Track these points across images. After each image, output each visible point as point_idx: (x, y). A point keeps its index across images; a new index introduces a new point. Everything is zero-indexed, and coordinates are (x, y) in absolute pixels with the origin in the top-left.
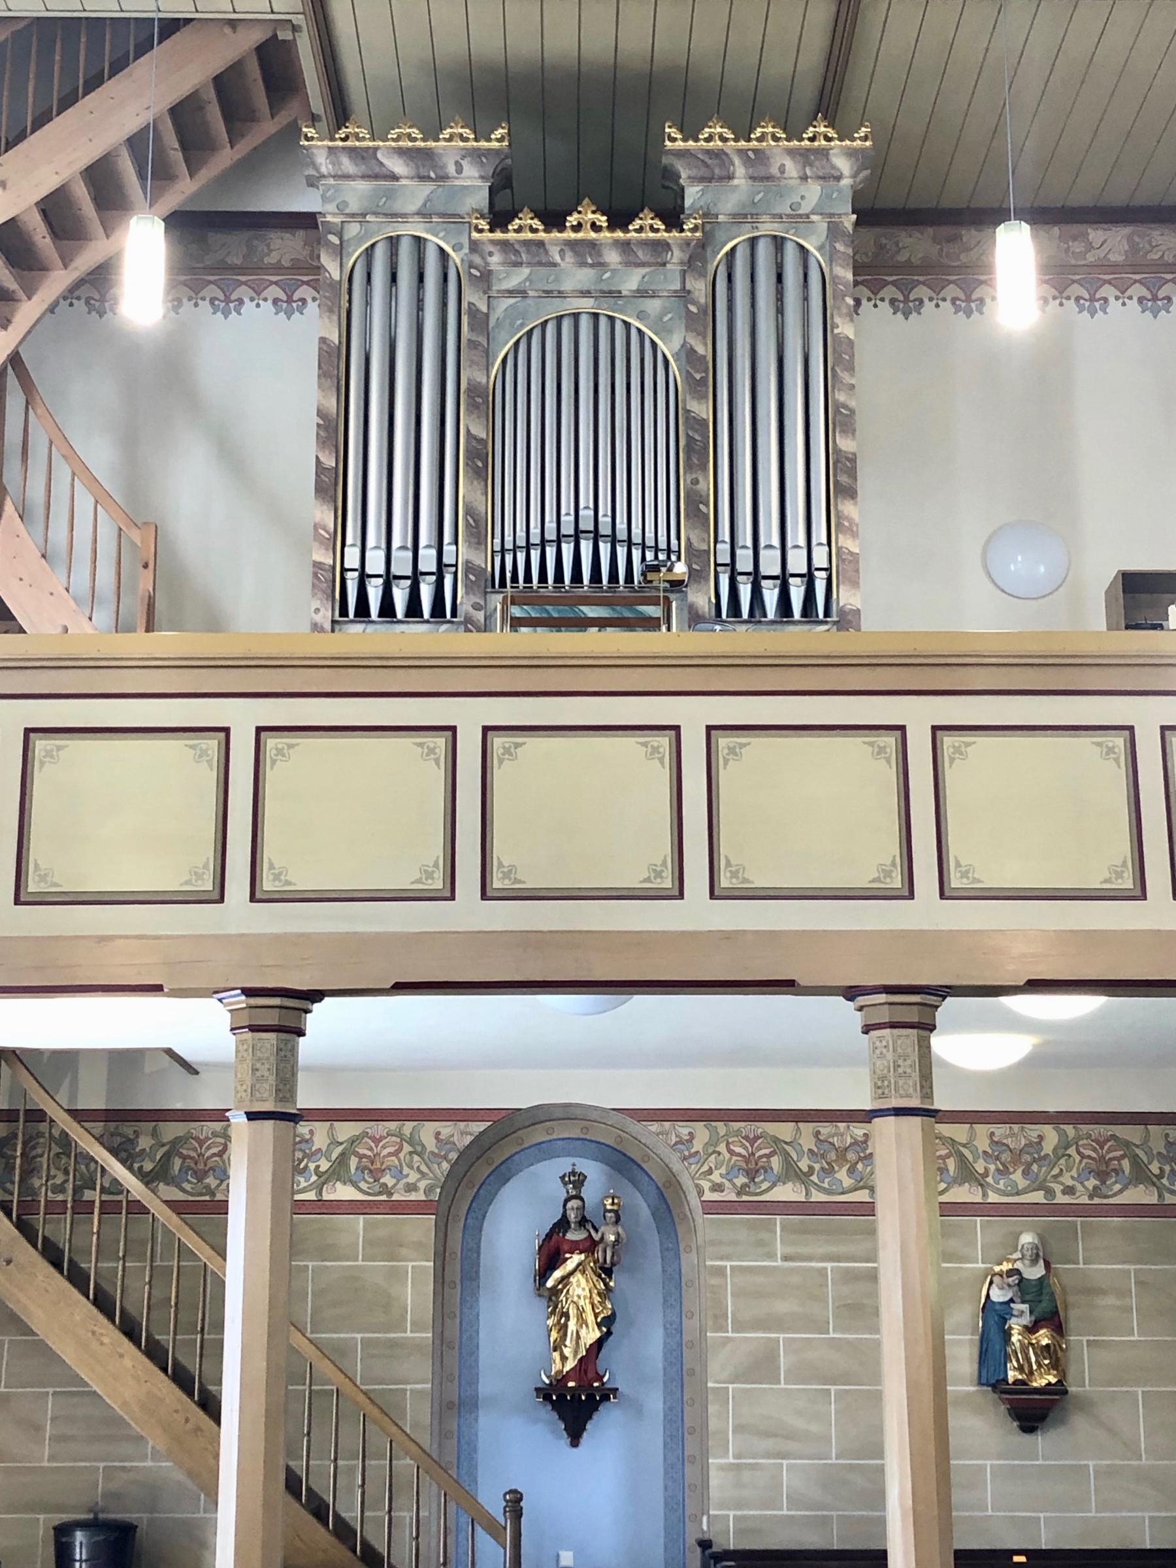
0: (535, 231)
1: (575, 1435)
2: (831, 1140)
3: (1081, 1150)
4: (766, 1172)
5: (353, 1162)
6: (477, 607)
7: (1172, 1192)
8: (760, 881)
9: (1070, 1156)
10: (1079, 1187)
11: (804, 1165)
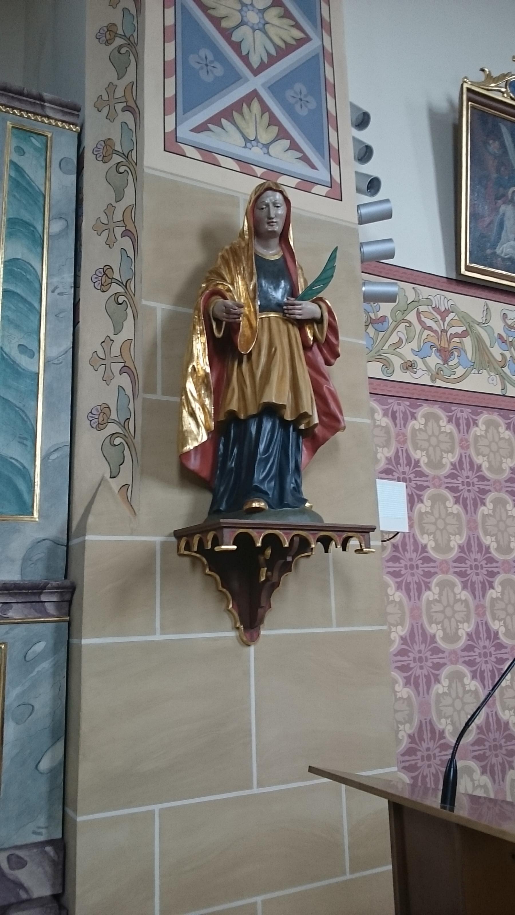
3: (423, 319)
7: (514, 384)
8: (174, 93)
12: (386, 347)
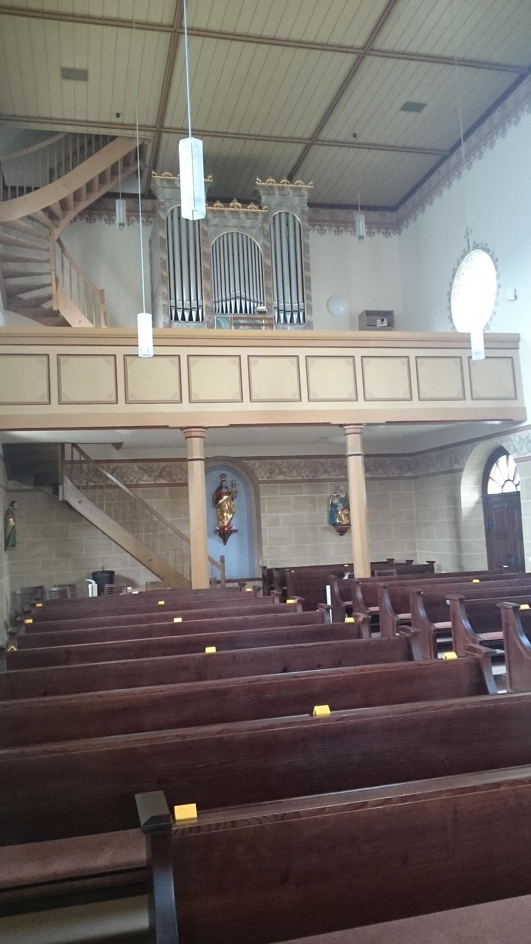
0: (221, 207)
1: (225, 541)
5: (164, 473)
6: (210, 318)
11: (284, 470)
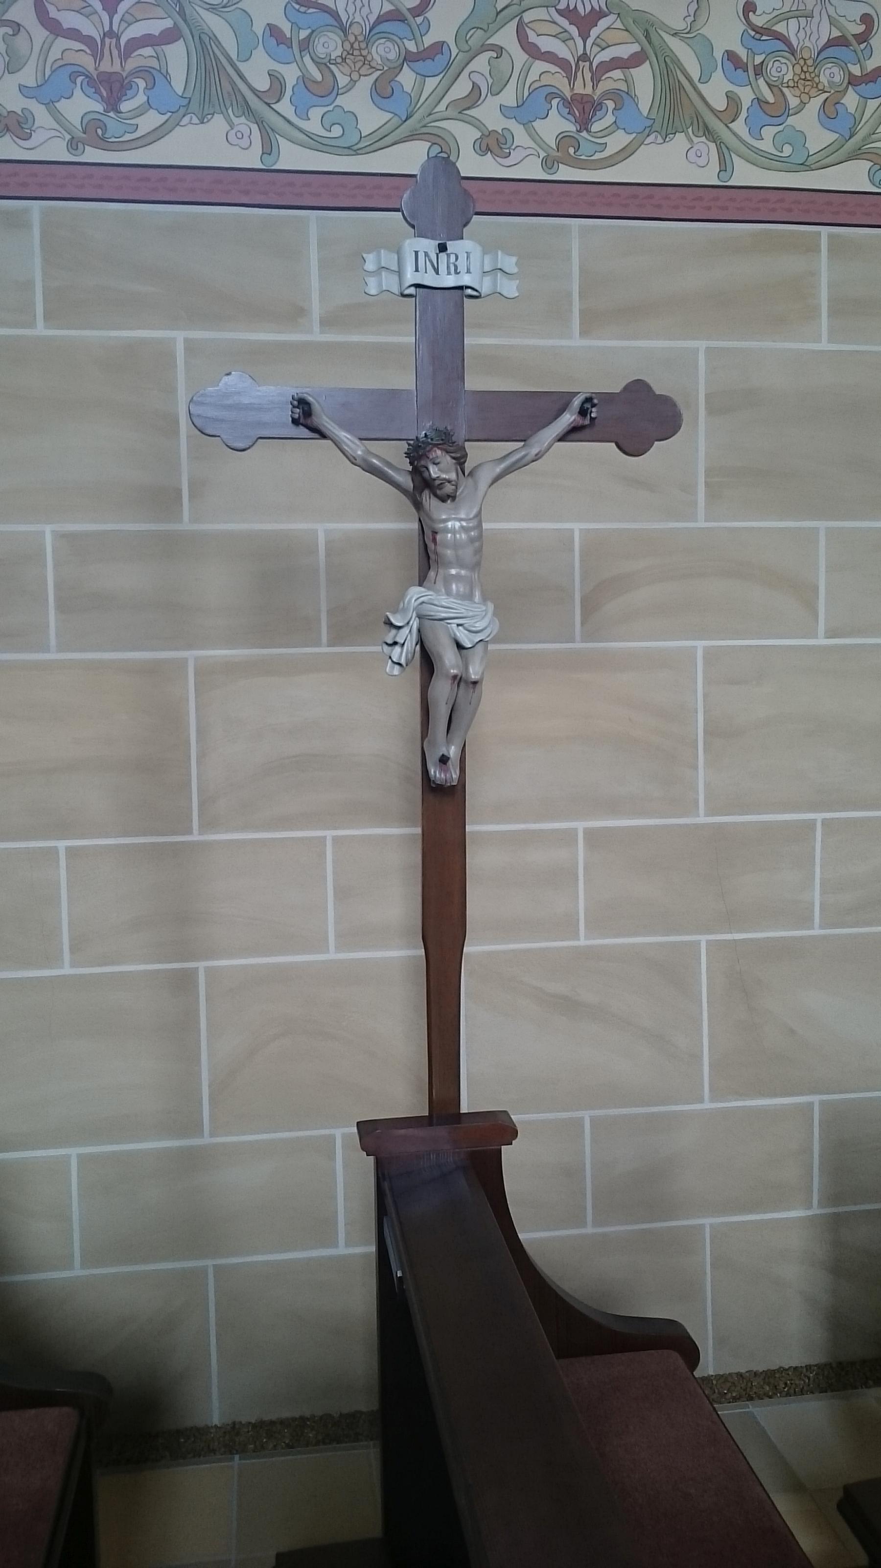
2: (780, 28)
3: (532, 37)
4: (151, 86)
9: (500, 51)
10: (521, 136)
12: (442, 107)
